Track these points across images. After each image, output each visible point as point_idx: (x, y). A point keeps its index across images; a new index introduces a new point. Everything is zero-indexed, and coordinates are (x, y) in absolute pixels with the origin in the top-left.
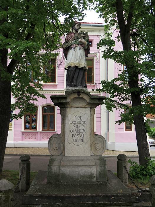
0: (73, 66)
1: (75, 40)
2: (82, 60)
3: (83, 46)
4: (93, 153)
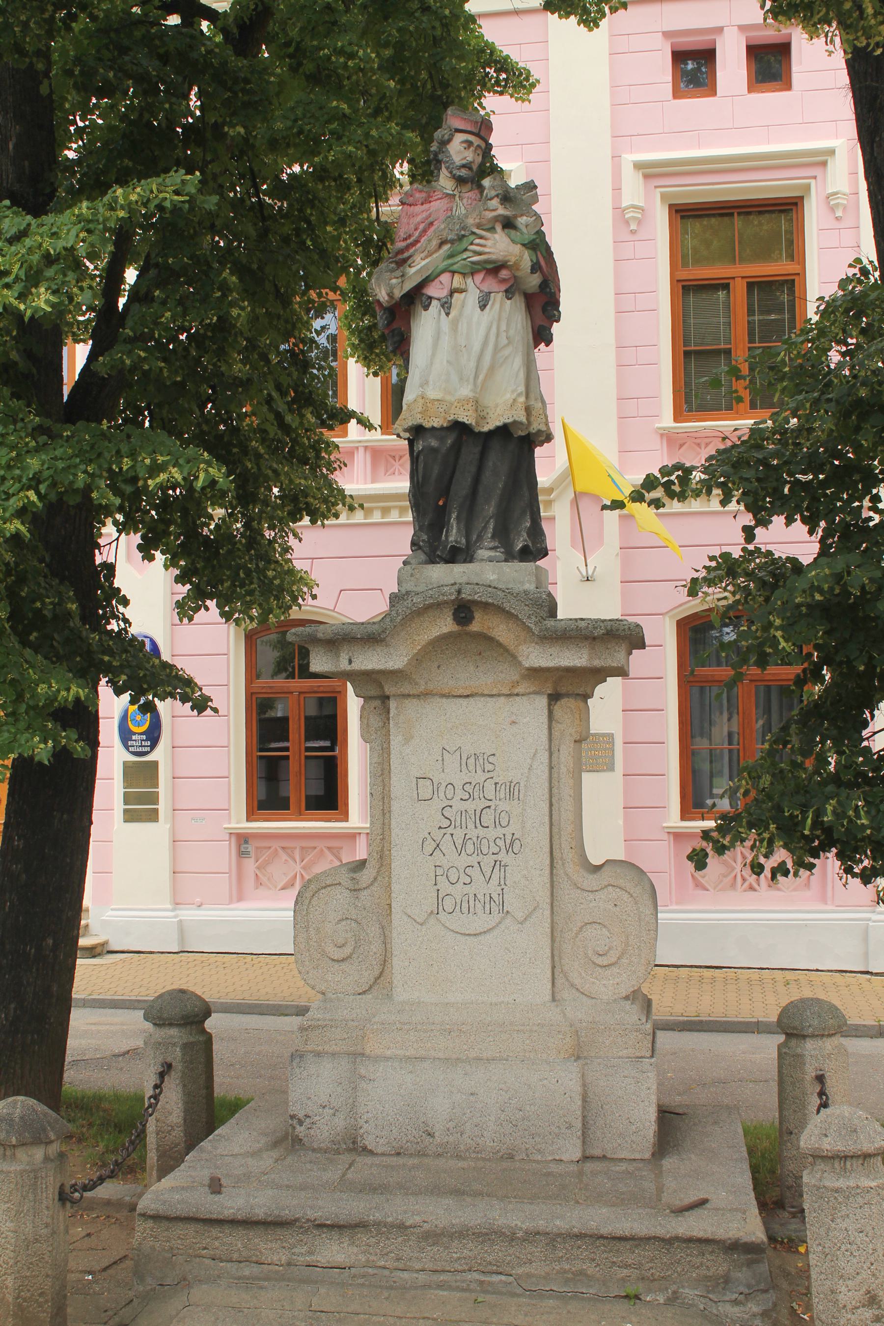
0: (436, 423)
1: (446, 247)
3: (504, 281)
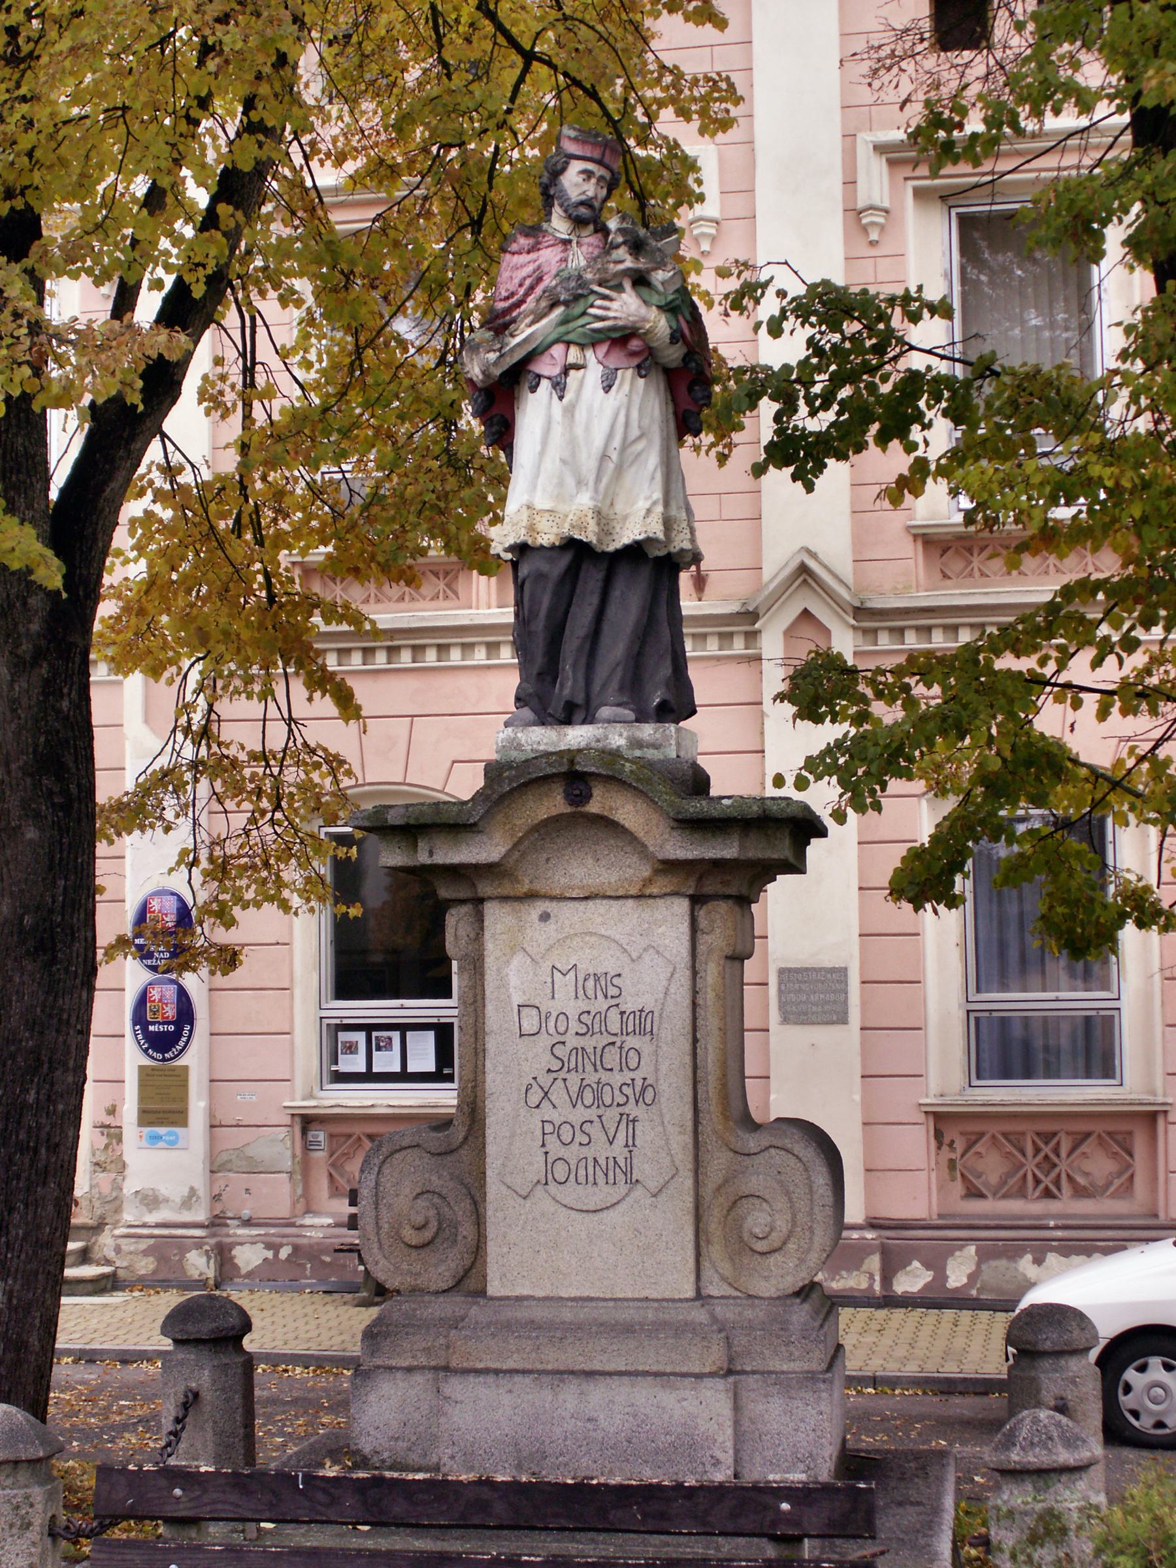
1: (559, 311)
2: (629, 476)
3: (633, 354)
4: (723, 1279)
